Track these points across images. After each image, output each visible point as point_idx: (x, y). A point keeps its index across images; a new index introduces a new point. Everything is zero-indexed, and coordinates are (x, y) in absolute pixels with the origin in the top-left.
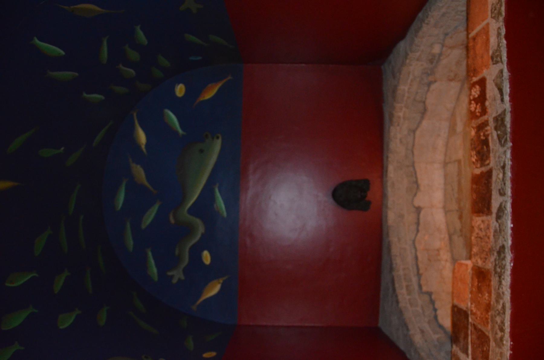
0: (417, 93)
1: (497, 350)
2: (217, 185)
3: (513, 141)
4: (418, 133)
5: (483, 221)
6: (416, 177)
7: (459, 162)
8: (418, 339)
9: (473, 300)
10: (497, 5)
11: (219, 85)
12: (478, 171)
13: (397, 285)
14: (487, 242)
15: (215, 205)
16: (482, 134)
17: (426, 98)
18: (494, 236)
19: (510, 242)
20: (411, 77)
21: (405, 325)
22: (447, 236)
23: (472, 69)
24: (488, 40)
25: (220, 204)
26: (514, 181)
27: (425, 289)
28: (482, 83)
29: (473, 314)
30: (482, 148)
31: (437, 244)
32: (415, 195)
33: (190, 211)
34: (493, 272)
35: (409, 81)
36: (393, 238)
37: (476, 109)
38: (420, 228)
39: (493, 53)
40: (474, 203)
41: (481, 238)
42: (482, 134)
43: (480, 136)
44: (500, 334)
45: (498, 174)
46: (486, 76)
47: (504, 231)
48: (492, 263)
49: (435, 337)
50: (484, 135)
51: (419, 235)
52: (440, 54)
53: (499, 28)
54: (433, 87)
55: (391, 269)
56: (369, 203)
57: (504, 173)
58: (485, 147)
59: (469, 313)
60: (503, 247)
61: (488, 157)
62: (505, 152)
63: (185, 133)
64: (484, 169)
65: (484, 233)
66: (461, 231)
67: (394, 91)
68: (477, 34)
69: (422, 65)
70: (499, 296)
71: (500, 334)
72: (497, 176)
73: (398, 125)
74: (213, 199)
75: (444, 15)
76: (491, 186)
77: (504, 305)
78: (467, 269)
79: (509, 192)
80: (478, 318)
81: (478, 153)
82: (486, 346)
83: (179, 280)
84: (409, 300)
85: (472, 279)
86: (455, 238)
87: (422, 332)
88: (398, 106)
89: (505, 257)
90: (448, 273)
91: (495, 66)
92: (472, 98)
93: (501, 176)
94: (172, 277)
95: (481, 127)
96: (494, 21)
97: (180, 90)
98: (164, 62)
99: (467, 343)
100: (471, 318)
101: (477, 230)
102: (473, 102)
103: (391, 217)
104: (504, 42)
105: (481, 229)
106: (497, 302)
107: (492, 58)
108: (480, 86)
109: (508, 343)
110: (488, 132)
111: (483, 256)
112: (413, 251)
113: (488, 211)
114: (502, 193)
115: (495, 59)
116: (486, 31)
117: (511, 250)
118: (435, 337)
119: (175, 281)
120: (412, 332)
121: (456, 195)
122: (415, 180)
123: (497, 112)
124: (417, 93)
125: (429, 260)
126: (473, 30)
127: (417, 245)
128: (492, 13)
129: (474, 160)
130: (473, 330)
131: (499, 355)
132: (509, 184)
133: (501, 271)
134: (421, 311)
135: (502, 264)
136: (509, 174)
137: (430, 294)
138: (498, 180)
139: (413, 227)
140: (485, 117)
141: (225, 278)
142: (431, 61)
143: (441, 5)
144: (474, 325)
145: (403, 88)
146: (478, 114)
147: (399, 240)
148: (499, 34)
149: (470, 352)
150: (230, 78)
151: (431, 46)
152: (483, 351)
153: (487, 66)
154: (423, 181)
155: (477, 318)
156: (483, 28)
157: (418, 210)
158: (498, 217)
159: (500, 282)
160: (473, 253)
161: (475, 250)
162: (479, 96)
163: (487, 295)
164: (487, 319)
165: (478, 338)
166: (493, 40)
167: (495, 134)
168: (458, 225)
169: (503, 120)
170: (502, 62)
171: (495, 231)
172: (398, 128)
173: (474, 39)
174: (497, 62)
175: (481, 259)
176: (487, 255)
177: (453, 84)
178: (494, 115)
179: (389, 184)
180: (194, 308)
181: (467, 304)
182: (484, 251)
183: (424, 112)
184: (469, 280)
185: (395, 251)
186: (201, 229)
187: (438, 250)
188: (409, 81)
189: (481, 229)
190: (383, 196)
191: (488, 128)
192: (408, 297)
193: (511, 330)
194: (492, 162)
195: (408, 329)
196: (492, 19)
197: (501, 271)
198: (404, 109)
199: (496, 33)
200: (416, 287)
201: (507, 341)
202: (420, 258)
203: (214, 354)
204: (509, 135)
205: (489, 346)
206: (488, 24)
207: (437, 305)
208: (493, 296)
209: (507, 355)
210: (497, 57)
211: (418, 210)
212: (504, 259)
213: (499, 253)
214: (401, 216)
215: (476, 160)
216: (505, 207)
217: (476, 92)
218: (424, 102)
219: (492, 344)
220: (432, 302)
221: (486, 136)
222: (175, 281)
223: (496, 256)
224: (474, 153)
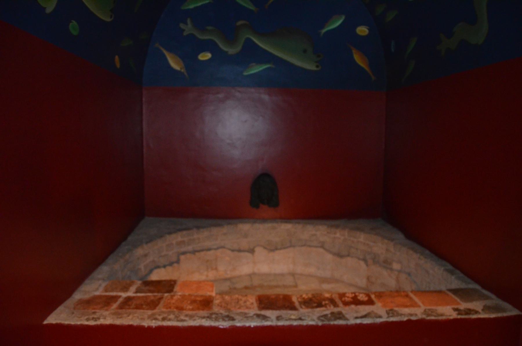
0: (357, 249)
1: (146, 316)
2: (273, 66)
3: (323, 326)
4: (321, 250)
5: (252, 304)
6: (281, 249)
7: (296, 286)
8: (140, 251)
9: (183, 296)
12: (294, 299)
13: (185, 232)
14: (235, 307)
15: (254, 64)
16: (327, 302)
17: (352, 257)
19: (239, 324)
21: (150, 240)
22: (228, 276)
24: (406, 306)
25: (256, 69)
26: (290, 327)
27: (182, 257)
28: (370, 302)
29: (172, 297)
30: (315, 303)
31: (222, 268)
32: (265, 248)
33: (248, 40)
34: (211, 312)
36: (225, 229)
37: (348, 297)
39: (395, 311)
40: (268, 297)
41: (238, 302)
42: (327, 302)
44: (160, 318)
45: (294, 315)
47: (247, 320)
49: (142, 266)
51: (229, 252)
52: (391, 269)
53: (416, 315)
54: (362, 263)
55: (198, 228)
56: (257, 207)
57: (295, 320)
59: (172, 294)
60: (233, 319)
61: (307, 307)
62: (314, 320)
63: (322, 34)
64: (297, 304)
65: (242, 304)
66: (235, 288)
68: (411, 298)
70: (191, 317)
71: (160, 318)
72: (294, 315)
73: (328, 233)
74: (260, 62)
75: (427, 272)
76: (283, 310)
79: (280, 323)
80: (169, 301)
81: (310, 300)
83: (183, 30)
85: (202, 296)
86: (228, 283)
87: (146, 255)
88: (346, 233)
90: (197, 277)
91: (385, 312)
92: (357, 294)
93: (293, 317)
94: (186, 24)
95: (332, 301)
97: (362, 30)
98: (391, 16)
99: (145, 292)
100: (168, 296)
101: (244, 299)
102: (353, 295)
103: (245, 227)
104: (405, 319)
105: (245, 302)
106: (186, 316)
107: (391, 310)
109: (154, 324)
111: (223, 304)
112: (215, 247)
113: (261, 308)
114: (278, 318)
115: (391, 312)
116: (414, 305)
117: (231, 326)
119: (182, 26)
120: (145, 246)
121: (265, 284)
124: (357, 249)
125: (208, 261)
127: (220, 250)
128: (429, 310)
129: (304, 296)
131: (142, 317)
132: (287, 323)
134: (163, 254)
136: (295, 323)
137: (178, 262)
140: (341, 305)
141: (186, 74)
142: (385, 261)
145: (362, 237)
146: (343, 299)
147: (225, 234)
148: (411, 315)
149: (139, 295)
150: (373, 78)
152: (142, 305)
153: (384, 306)
154: (278, 255)
155: (168, 300)
157: (252, 251)
158: (258, 316)
160: (224, 296)
161: (227, 298)
162: (359, 300)
163: (191, 307)
164: (170, 308)
165: (152, 301)
166: (406, 311)
167: (328, 312)
168: (239, 286)
169: (340, 318)
170: (388, 317)
171: (246, 314)
174: (388, 313)
175: (221, 302)
176: (224, 307)
177: (365, 281)
179: (275, 225)
180: (157, 45)
181: (179, 292)
182: (227, 304)
183: (340, 255)
184: (200, 293)
185: (215, 230)
186: (232, 51)
187: (216, 269)
189: (245, 302)
190: (264, 220)
191: (332, 307)
194: (304, 311)
195: (147, 243)
199: (413, 312)
200: (183, 249)
202: (209, 253)
203: (118, 65)
205: (147, 309)
206: (419, 306)
207: (169, 268)
208: (190, 313)
210: (393, 313)
211: (252, 251)
212: (224, 320)
213: (228, 316)
214: (246, 236)
215: (304, 298)
217: (362, 297)
218: (348, 255)
219: (150, 312)
220: (171, 264)
221: (325, 306)
222: (182, 26)
224: (310, 296)
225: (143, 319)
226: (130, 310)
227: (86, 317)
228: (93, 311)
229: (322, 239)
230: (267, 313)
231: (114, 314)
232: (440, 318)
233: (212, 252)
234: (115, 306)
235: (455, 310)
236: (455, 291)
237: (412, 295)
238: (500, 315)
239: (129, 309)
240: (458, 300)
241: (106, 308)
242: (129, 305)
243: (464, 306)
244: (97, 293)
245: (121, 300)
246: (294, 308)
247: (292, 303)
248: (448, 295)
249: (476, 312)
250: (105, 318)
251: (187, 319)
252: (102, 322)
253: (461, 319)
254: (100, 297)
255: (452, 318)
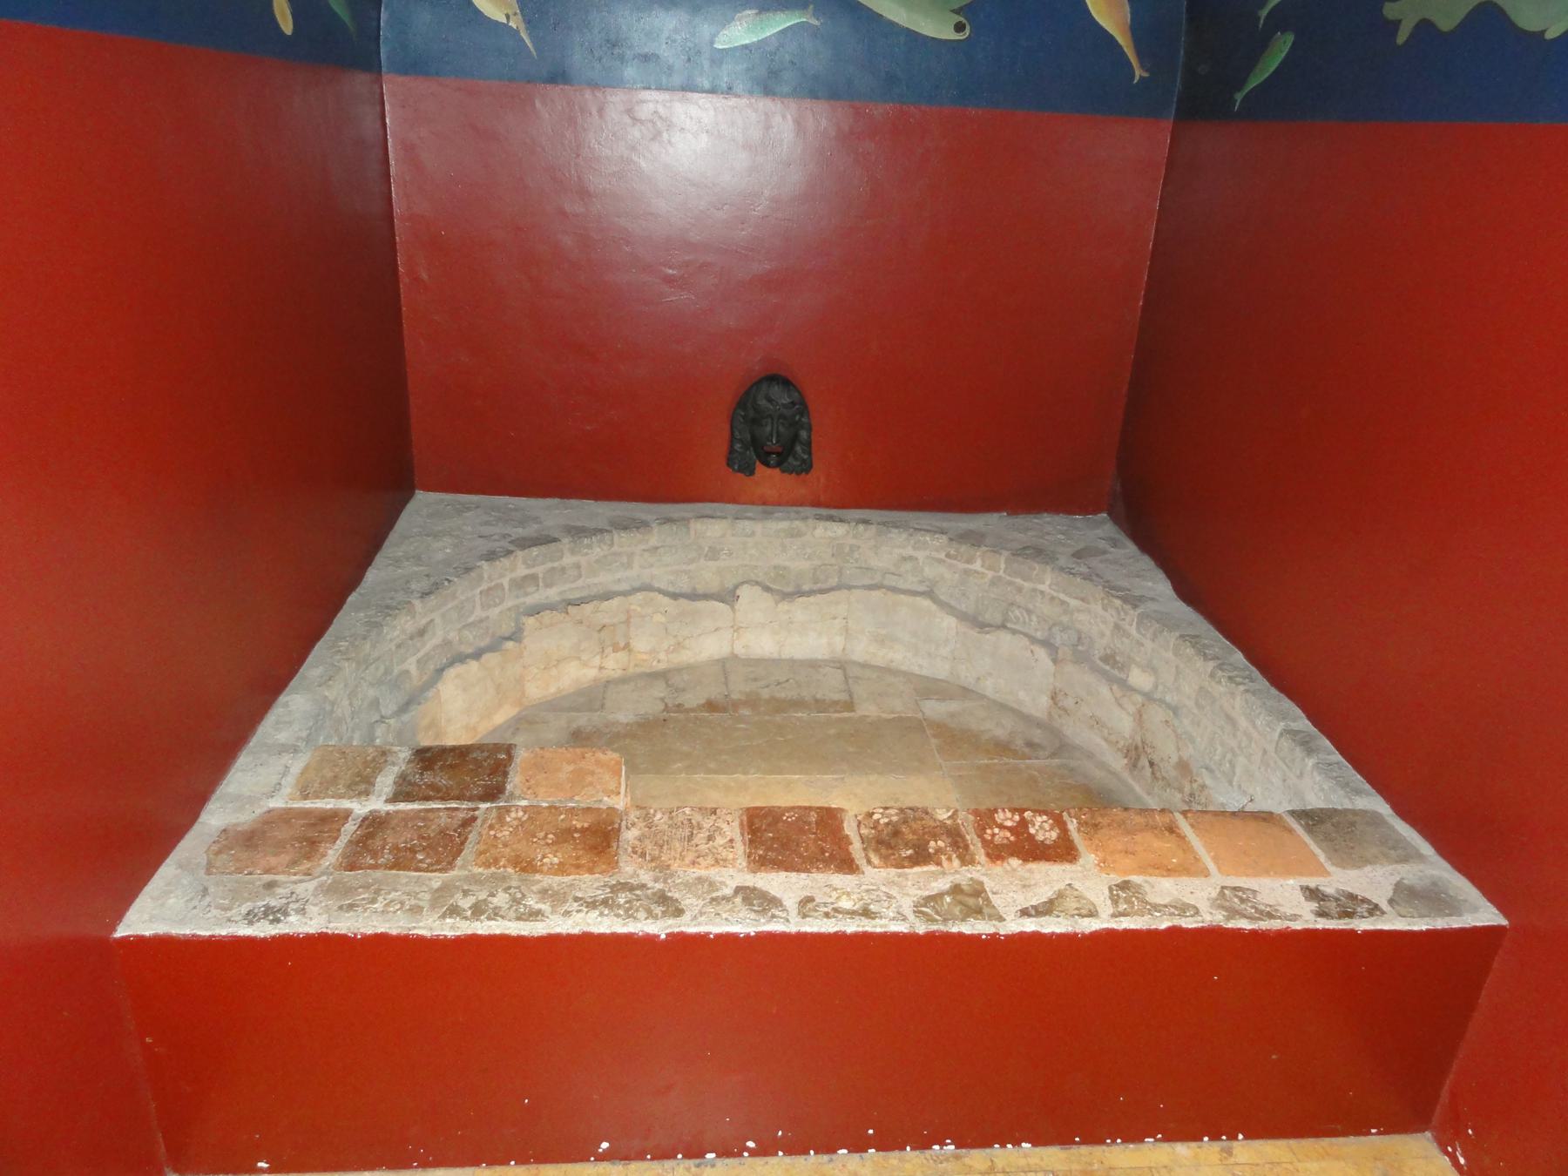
0: (1029, 612)
3: (930, 936)
4: (926, 603)
7: (849, 706)
10: (1252, 907)
11: (1123, 40)
12: (849, 829)
13: (535, 551)
14: (682, 858)
17: (1014, 632)
18: (700, 880)
20: (1074, 603)
22: (662, 666)
23: (1100, 819)
24: (1169, 872)
30: (907, 846)
31: (642, 644)
32: (767, 589)
35: (1062, 596)
37: (1002, 827)
38: (682, 601)
43: (935, 837)
46: (1081, 861)
48: (635, 875)
49: (411, 665)
50: (939, 851)
51: (666, 600)
52: (1124, 684)
54: (1042, 653)
57: (852, 913)
58: (910, 852)
61: (887, 861)
64: (856, 848)
65: (703, 847)
66: (679, 707)
67: (1039, 553)
69: (1102, 635)
70: (556, 898)
71: (466, 903)
73: (948, 555)
75: (1231, 720)
77: (540, 917)
78: (609, 793)
82: (428, 861)
84: (500, 586)
86: (659, 690)
87: (422, 633)
89: (656, 917)
92: (1027, 814)
93: (846, 904)
96: (1214, 894)
99: (427, 799)
105: (710, 838)
106: (544, 894)
107: (1125, 886)
108: (1056, 844)
110: (945, 863)
112: (624, 587)
116: (1190, 868)
118: (411, 665)
122: (806, 588)
123: (994, 893)
124: (1029, 612)
126: (1192, 826)
127: (640, 596)
130: (461, 815)
133: (619, 906)
135: (637, 911)
136: (851, 927)
137: (516, 636)
138: (834, 895)
139: (684, 585)
140: (981, 856)
142: (1107, 659)
143: (1258, 722)
144: (474, 819)
145: (1047, 580)
150: (1139, 73)
151: (1150, 668)
152: (413, 850)
154: (799, 610)
155: (491, 827)
156: (1197, 859)
159: (592, 905)
162: (1031, 838)
164: (496, 861)
167: (942, 884)
169: (978, 912)
172: (942, 556)
173: (1172, 829)
177: (1045, 701)
178: (989, 885)
184: (581, 800)
185: (623, 541)
187: (627, 647)
188: (1062, 596)
192: (505, 582)
193: (481, 936)
194: (875, 875)
196: (1218, 890)
197: (619, 906)
198: (990, 574)
200: (536, 597)
201: (452, 928)
204: (942, 928)
209: (420, 928)
211: (728, 596)
214: (714, 554)
216: (773, 916)
218: (1003, 626)
219: (436, 880)
223: (653, 888)
225: (416, 910)
226: (378, 874)
227: (244, 909)
228: (268, 878)
229: (929, 572)
230: (774, 882)
231: (330, 890)
232: (1264, 925)
233: (615, 602)
234: (333, 854)
235: (1313, 894)
236: (1312, 819)
237: (1184, 825)
238: (1440, 923)
239: (375, 867)
240: (1322, 857)
241: (306, 865)
242: (375, 854)
243: (1339, 880)
244: (277, 803)
245: (350, 828)
246: (847, 865)
247: (842, 841)
248: (1290, 831)
249: (1374, 910)
250: (302, 911)
251: (546, 907)
252: (297, 925)
253: (1327, 933)
254: (286, 817)
255: (1297, 926)
